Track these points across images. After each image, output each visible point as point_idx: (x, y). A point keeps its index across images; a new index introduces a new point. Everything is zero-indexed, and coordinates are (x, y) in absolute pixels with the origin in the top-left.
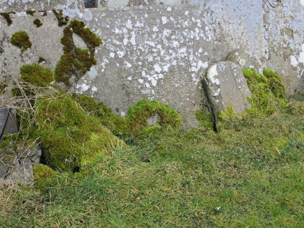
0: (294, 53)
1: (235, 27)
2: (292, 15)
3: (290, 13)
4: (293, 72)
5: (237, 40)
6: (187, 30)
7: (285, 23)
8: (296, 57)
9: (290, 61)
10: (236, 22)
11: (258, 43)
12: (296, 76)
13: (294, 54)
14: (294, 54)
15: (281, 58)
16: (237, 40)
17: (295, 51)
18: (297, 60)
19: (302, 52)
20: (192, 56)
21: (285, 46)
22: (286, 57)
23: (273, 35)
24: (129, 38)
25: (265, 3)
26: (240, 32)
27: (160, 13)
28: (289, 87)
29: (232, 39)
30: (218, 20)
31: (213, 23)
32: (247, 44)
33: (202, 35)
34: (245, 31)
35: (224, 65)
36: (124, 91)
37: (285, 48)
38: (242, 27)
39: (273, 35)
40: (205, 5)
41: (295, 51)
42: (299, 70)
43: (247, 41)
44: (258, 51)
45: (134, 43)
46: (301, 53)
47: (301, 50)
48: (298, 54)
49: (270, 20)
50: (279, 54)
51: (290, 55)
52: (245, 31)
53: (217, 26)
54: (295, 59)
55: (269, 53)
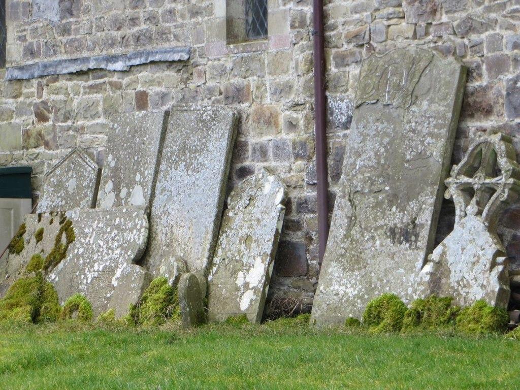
0: (244, 268)
1: (185, 231)
2: (260, 218)
3: (259, 216)
4: (234, 293)
5: (183, 246)
6: (128, 231)
7: (249, 228)
8: (244, 274)
9: (236, 278)
10: (187, 225)
11: (201, 250)
12: (235, 298)
13: (244, 269)
14: (244, 269)
15: (228, 274)
16: (183, 246)
17: (246, 266)
18: (245, 278)
19: (253, 267)
20: (122, 257)
21: (238, 258)
22: (234, 273)
23: (231, 243)
24: (90, 237)
25: (237, 202)
26: (187, 237)
27: (118, 214)
28: (223, 311)
29: (179, 245)
30: (172, 223)
31: (167, 226)
32: (191, 251)
33: (136, 237)
34: (194, 235)
35: (131, 268)
36: (70, 284)
37: (237, 261)
38: (190, 232)
39: (231, 243)
40: (165, 206)
41: (246, 266)
42: (242, 292)
43: (191, 248)
44: (199, 261)
45: (91, 242)
46: (252, 269)
47: (253, 265)
48: (248, 270)
49: (235, 224)
50: (228, 268)
51: (239, 270)
52: (193, 236)
53: (169, 230)
54: (243, 275)
55: (219, 266)
